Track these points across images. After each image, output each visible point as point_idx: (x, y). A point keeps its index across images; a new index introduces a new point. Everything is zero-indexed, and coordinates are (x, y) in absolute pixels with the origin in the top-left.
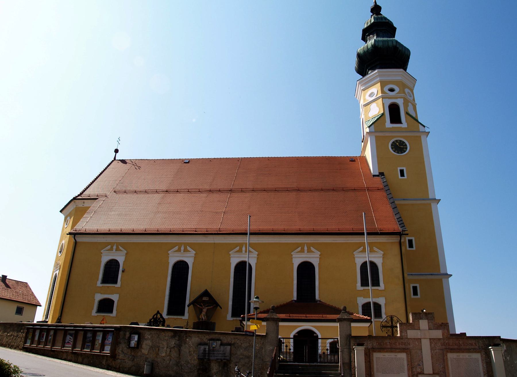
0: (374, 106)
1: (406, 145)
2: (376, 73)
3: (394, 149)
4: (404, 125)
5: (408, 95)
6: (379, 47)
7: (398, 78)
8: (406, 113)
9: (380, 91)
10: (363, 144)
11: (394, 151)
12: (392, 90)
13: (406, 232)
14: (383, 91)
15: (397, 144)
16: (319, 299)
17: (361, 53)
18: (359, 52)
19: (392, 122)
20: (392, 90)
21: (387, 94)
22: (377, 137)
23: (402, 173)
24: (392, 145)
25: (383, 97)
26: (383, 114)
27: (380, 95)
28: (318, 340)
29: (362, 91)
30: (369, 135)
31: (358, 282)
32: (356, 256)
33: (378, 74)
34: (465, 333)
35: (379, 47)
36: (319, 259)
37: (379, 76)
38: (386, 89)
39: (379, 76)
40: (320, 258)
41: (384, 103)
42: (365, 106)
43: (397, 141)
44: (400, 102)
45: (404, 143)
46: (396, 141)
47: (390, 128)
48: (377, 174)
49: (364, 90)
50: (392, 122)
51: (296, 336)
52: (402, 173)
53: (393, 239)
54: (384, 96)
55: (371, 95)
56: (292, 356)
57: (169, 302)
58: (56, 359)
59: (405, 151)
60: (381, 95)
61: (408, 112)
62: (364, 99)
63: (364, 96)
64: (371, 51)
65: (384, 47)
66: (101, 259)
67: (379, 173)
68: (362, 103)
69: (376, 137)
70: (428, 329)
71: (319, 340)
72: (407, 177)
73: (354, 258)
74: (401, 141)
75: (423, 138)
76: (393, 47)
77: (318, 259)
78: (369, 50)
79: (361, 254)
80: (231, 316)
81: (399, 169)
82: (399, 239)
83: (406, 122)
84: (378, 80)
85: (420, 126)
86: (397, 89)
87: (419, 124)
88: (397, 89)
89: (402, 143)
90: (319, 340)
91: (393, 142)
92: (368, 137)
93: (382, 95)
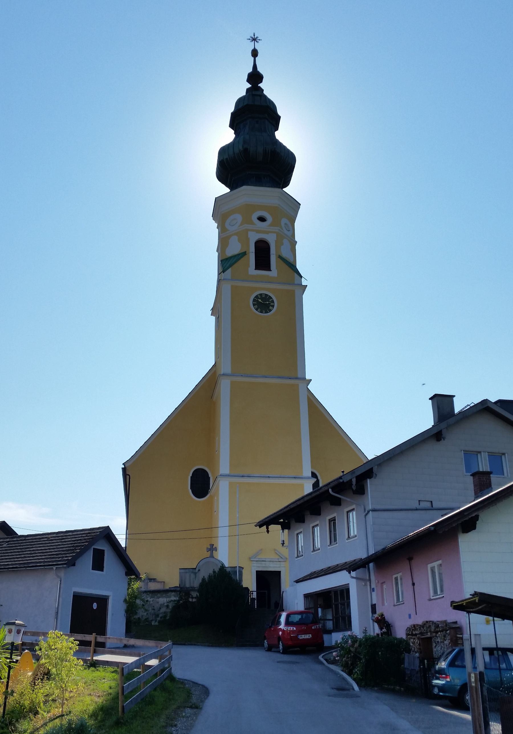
4: (274, 272)
5: (284, 229)
11: (257, 310)
15: (260, 300)
19: (258, 267)
28: (256, 590)
43: (257, 297)
44: (271, 239)
46: (260, 294)
50: (258, 267)
51: (156, 625)
56: (433, 640)
58: (210, 482)
61: (280, 255)
66: (154, 659)
70: (482, 452)
71: (256, 590)
80: (282, 573)
90: (256, 590)
91: (254, 300)
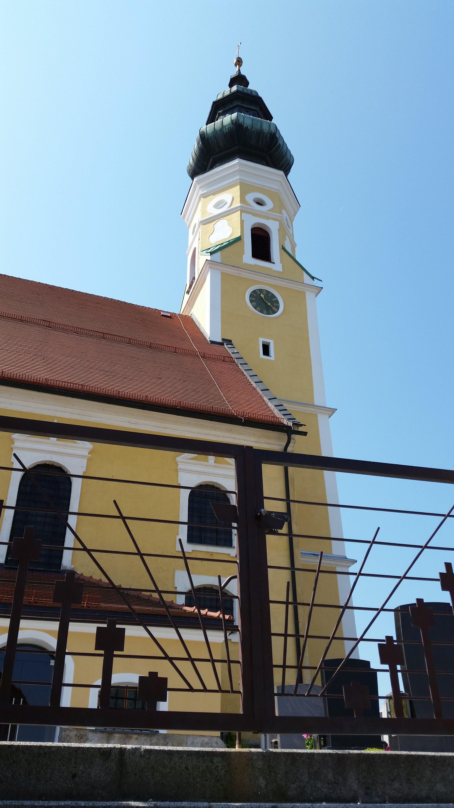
0: (222, 224)
1: (277, 302)
2: (234, 165)
3: (254, 303)
6: (245, 126)
7: (275, 186)
8: (281, 247)
9: (238, 199)
10: (187, 297)
11: (255, 308)
12: (260, 203)
13: (301, 429)
14: (243, 200)
15: (262, 296)
16: (73, 566)
17: (208, 132)
18: (204, 131)
20: (260, 203)
21: (251, 206)
22: (224, 276)
23: (266, 350)
24: (251, 296)
25: (244, 209)
26: (238, 239)
27: (237, 204)
29: (202, 198)
30: (210, 268)
31: (180, 531)
32: (180, 466)
33: (238, 168)
34: (156, 673)
35: (245, 126)
36: (86, 460)
37: (240, 172)
38: (250, 198)
39: (240, 172)
40: (89, 460)
41: (243, 221)
42: (204, 224)
43: (261, 290)
45: (275, 297)
47: (250, 265)
48: (220, 340)
49: (205, 196)
50: (255, 255)
52: (266, 350)
53: (269, 441)
54: (245, 208)
55: (218, 205)
57: (84, 726)
59: (274, 312)
60: (240, 205)
62: (204, 212)
63: (204, 206)
64: (227, 131)
65: (253, 130)
67: (223, 339)
68: (198, 218)
69: (223, 274)
72: (275, 358)
73: (177, 471)
74: (268, 292)
75: (309, 296)
76: (269, 135)
77: (85, 461)
78: (224, 129)
79: (196, 464)
81: (261, 340)
82: (285, 444)
83: (281, 263)
84: (236, 180)
85: (306, 276)
86: (269, 204)
87: (304, 272)
88: (269, 204)
89: (271, 297)
91: (254, 292)
92: (208, 272)
93: (241, 206)
